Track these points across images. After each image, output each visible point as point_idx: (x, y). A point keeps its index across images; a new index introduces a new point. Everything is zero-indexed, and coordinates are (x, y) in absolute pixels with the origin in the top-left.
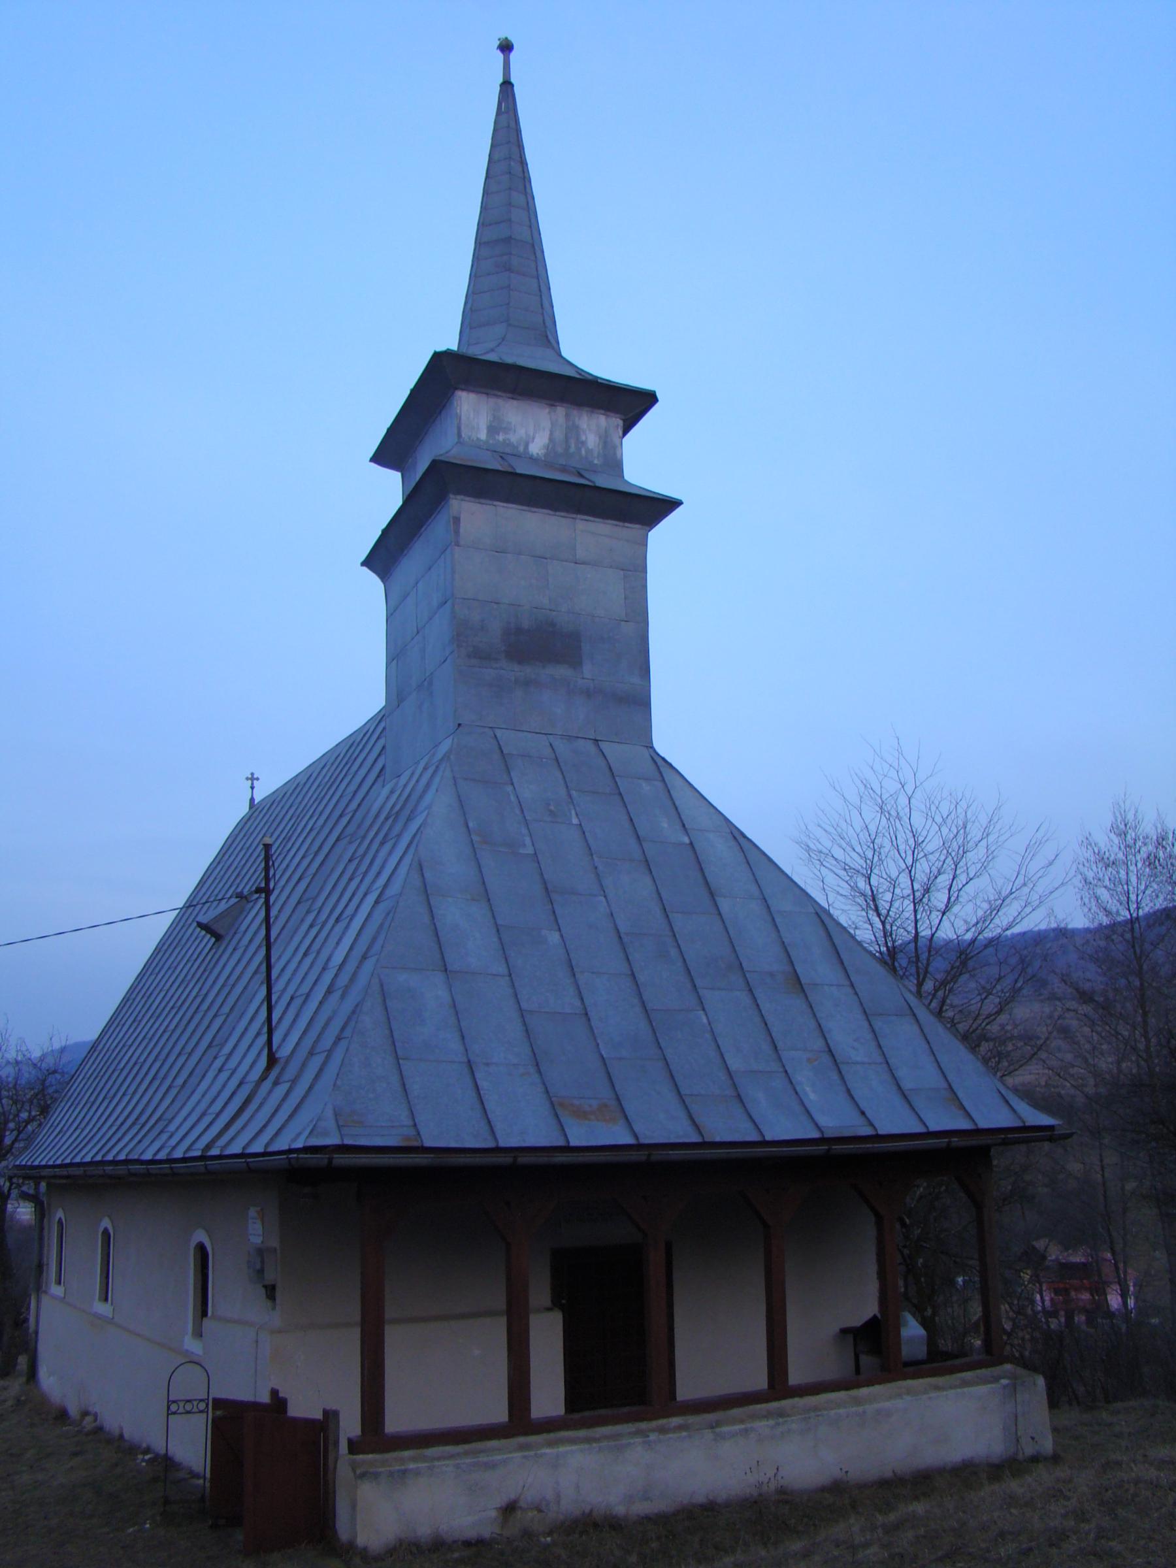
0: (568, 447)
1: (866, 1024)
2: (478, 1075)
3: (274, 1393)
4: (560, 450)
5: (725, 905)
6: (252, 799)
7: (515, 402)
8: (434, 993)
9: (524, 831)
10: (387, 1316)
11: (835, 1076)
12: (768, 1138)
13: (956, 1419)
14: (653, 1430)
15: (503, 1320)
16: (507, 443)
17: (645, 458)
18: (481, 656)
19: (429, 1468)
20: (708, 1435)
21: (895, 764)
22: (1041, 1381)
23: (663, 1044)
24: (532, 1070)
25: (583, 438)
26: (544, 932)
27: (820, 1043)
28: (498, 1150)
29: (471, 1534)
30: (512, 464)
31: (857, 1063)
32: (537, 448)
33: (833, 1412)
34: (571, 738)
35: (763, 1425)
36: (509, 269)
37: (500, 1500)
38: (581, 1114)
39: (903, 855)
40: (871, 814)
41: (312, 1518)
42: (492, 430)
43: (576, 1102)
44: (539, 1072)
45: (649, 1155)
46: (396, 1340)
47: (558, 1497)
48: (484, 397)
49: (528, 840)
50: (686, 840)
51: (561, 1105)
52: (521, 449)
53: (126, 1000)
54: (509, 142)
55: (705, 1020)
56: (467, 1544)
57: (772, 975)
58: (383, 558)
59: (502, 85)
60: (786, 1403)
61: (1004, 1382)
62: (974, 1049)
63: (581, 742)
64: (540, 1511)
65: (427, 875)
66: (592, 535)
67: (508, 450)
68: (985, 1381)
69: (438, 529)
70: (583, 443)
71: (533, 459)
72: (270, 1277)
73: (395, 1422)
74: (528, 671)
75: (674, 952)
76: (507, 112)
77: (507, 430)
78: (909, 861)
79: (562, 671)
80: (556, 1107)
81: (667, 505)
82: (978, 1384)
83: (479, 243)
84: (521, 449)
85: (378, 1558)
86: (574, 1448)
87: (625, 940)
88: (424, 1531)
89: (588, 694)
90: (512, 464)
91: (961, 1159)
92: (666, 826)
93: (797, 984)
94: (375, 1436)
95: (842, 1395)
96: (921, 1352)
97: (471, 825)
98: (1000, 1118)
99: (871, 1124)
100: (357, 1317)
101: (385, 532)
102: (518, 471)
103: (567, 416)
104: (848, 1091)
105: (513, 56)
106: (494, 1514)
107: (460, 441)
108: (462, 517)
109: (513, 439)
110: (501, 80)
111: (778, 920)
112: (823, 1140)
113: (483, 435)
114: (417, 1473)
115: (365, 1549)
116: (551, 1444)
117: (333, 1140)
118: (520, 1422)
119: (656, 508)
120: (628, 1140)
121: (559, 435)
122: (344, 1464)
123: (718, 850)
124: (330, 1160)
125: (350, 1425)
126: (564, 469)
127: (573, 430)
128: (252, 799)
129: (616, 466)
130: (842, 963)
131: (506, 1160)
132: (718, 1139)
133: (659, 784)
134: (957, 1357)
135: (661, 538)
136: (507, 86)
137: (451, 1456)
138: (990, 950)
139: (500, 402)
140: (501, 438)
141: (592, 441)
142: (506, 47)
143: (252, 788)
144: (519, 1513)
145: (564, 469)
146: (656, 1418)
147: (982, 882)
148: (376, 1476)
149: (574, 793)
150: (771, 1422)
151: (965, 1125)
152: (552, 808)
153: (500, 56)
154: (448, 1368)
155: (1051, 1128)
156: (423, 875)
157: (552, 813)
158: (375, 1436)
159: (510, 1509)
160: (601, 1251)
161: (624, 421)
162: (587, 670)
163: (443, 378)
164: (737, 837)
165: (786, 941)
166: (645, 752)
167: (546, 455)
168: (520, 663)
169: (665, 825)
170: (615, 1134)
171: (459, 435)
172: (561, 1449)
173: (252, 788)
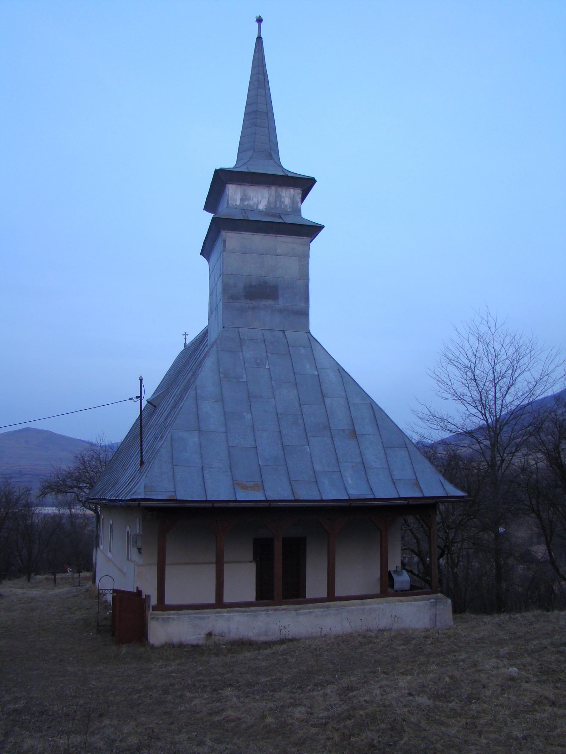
0: (276, 205)
1: (383, 452)
2: (205, 472)
3: (137, 588)
4: (272, 206)
5: (328, 401)
6: (185, 343)
7: (253, 187)
8: (193, 439)
9: (244, 372)
10: (166, 562)
11: (363, 474)
12: (324, 499)
13: (414, 614)
14: (271, 610)
15: (215, 565)
16: (248, 205)
17: (310, 210)
18: (234, 298)
19: (179, 618)
20: (294, 613)
21: (485, 318)
22: (449, 601)
23: (287, 460)
24: (228, 470)
25: (283, 200)
26: (245, 414)
27: (359, 460)
28: (207, 501)
29: (195, 642)
30: (258, 212)
31: (374, 468)
32: (262, 207)
33: (350, 608)
34: (272, 330)
35: (318, 611)
36: (256, 126)
37: (206, 631)
38: (245, 488)
39: (490, 361)
40: (473, 340)
41: (140, 634)
42: (242, 200)
43: (244, 483)
44: (231, 471)
45: (270, 505)
46: (169, 571)
47: (230, 632)
48: (239, 186)
49: (245, 376)
50: (316, 373)
51: (238, 484)
52: (255, 207)
53: (131, 430)
54: (259, 66)
55: (308, 450)
56: (193, 646)
57: (343, 430)
58: (206, 251)
59: (257, 38)
60: (332, 603)
61: (432, 600)
62: (432, 463)
63: (277, 332)
64: (222, 636)
65: (198, 391)
66: (285, 243)
67: (249, 208)
68: (424, 600)
69: (219, 245)
70: (283, 202)
71: (260, 212)
72: (139, 545)
73: (338, 594)
74: (254, 303)
75: (300, 421)
76: (258, 51)
77: (249, 200)
78: (493, 364)
79: (270, 302)
80: (236, 484)
81: (319, 228)
82: (421, 600)
83: (246, 114)
84: (255, 207)
85: (158, 648)
86: (237, 614)
87: (280, 416)
88: (176, 640)
89: (281, 311)
90: (258, 212)
91: (422, 508)
92: (309, 369)
93: (354, 434)
94: (162, 606)
95: (376, 600)
96: (407, 587)
97: (221, 370)
98: (438, 492)
99: (373, 494)
100: (215, 560)
101: (204, 243)
102: (250, 219)
103: (276, 191)
104: (368, 480)
105: (262, 24)
106: (203, 636)
107: (228, 207)
108: (227, 240)
109: (251, 203)
110: (257, 36)
111: (351, 407)
112: (267, 501)
113: (238, 203)
114: (173, 619)
115: (153, 645)
116: (228, 612)
117: (142, 496)
118: (220, 603)
119: (313, 230)
120: (263, 498)
121: (272, 200)
122: (150, 613)
123: (331, 376)
124: (139, 504)
125: (154, 601)
126: (273, 215)
127: (278, 197)
128: (185, 343)
129: (298, 211)
130: (377, 425)
131: (210, 505)
132: (302, 499)
133: (309, 349)
134: (422, 589)
135: (317, 246)
136: (259, 39)
137: (189, 614)
138: (530, 406)
139: (246, 187)
140: (246, 203)
141: (287, 201)
142: (259, 20)
143: (185, 339)
144: (213, 637)
145: (273, 215)
146: (276, 606)
147: (527, 375)
148: (158, 619)
149: (269, 355)
150: (322, 610)
151: (418, 495)
152: (258, 361)
153: (257, 24)
154: (190, 582)
155: (463, 497)
156: (196, 392)
157: (258, 364)
158: (162, 606)
159: (210, 635)
160: (281, 541)
161: (302, 191)
162: (281, 301)
163: (222, 179)
164: (341, 371)
165: (353, 416)
166: (306, 335)
167: (266, 209)
168: (251, 300)
169: (308, 367)
170: (259, 496)
171: (228, 204)
172: (232, 614)
173: (185, 339)
